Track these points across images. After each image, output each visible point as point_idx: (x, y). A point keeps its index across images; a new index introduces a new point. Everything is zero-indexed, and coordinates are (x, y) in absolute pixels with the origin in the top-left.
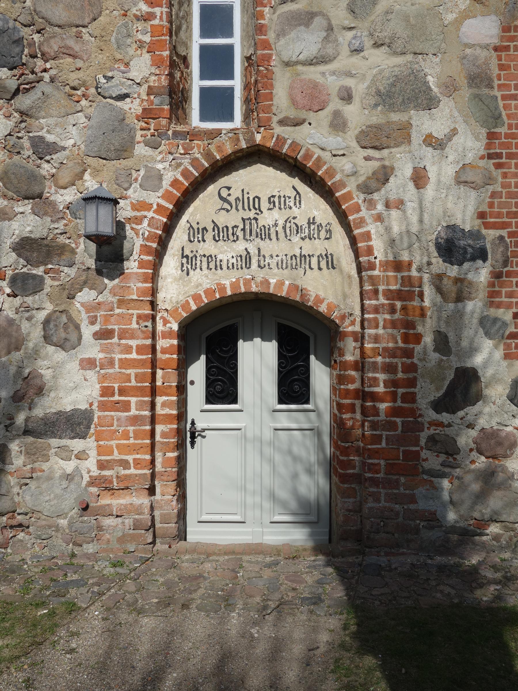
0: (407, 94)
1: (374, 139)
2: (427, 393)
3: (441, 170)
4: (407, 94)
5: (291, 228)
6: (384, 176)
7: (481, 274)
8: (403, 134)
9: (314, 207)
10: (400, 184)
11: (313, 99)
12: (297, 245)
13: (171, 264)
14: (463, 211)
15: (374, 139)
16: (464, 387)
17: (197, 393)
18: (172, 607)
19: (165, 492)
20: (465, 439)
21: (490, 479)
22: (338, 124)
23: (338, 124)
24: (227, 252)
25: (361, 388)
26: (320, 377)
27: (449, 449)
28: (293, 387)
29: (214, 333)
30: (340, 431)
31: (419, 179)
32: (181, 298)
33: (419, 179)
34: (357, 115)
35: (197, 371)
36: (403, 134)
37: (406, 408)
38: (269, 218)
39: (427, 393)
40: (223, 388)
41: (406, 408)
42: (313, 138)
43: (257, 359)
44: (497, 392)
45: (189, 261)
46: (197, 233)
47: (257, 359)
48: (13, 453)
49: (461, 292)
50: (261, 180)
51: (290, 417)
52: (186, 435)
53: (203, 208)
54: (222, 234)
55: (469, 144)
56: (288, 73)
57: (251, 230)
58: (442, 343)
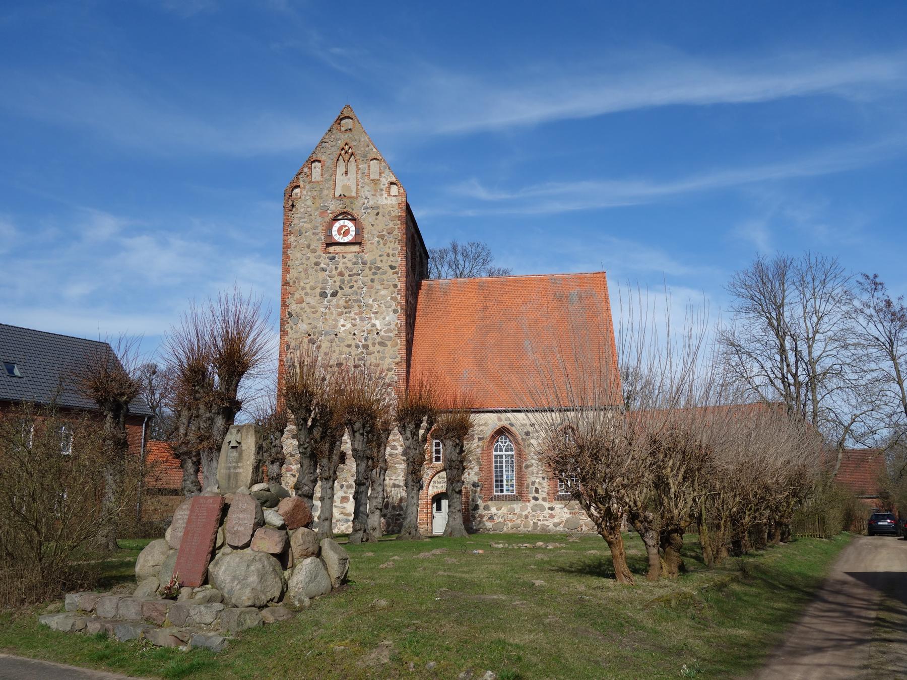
2: (471, 508)
3: (473, 473)
7: (479, 489)
13: (430, 488)
16: (476, 507)
17: (434, 509)
18: (243, 675)
19: (429, 525)
20: (477, 515)
27: (474, 517)
35: (434, 505)
39: (471, 508)
40: (439, 509)
44: (481, 508)
45: (433, 487)
46: (435, 482)
48: (707, 574)
49: (475, 492)
52: (433, 517)
58: (473, 500)
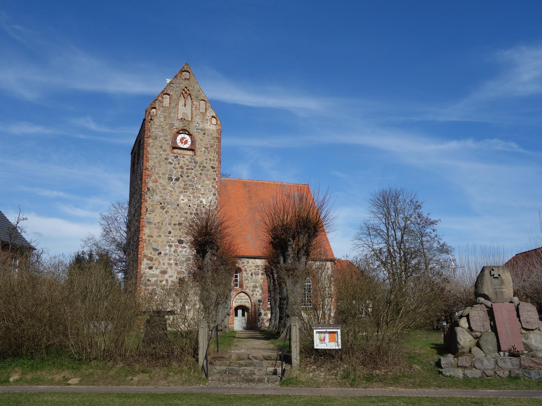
0: (255, 287)
1: (252, 291)
2: (257, 315)
3: (258, 294)
4: (255, 287)
5: (245, 299)
6: (253, 294)
7: (262, 303)
8: (255, 291)
9: (247, 297)
10: (255, 295)
11: (247, 287)
12: (245, 301)
14: (260, 297)
15: (252, 291)
20: (260, 319)
21: (262, 323)
22: (249, 289)
23: (249, 289)
24: (239, 301)
25: (522, 303)
26: (246, 314)
27: (259, 320)
28: (243, 315)
29: (236, 309)
30: (248, 318)
31: (256, 295)
32: (533, 348)
33: (256, 295)
34: (251, 289)
36: (255, 291)
37: (255, 316)
38: (243, 298)
39: (257, 315)
40: (236, 315)
41: (255, 316)
42: (247, 291)
43: (240, 312)
47: (240, 312)
50: (242, 294)
51: (243, 318)
53: (237, 297)
54: (239, 299)
55: (261, 291)
56: (318, 335)
57: (241, 299)
